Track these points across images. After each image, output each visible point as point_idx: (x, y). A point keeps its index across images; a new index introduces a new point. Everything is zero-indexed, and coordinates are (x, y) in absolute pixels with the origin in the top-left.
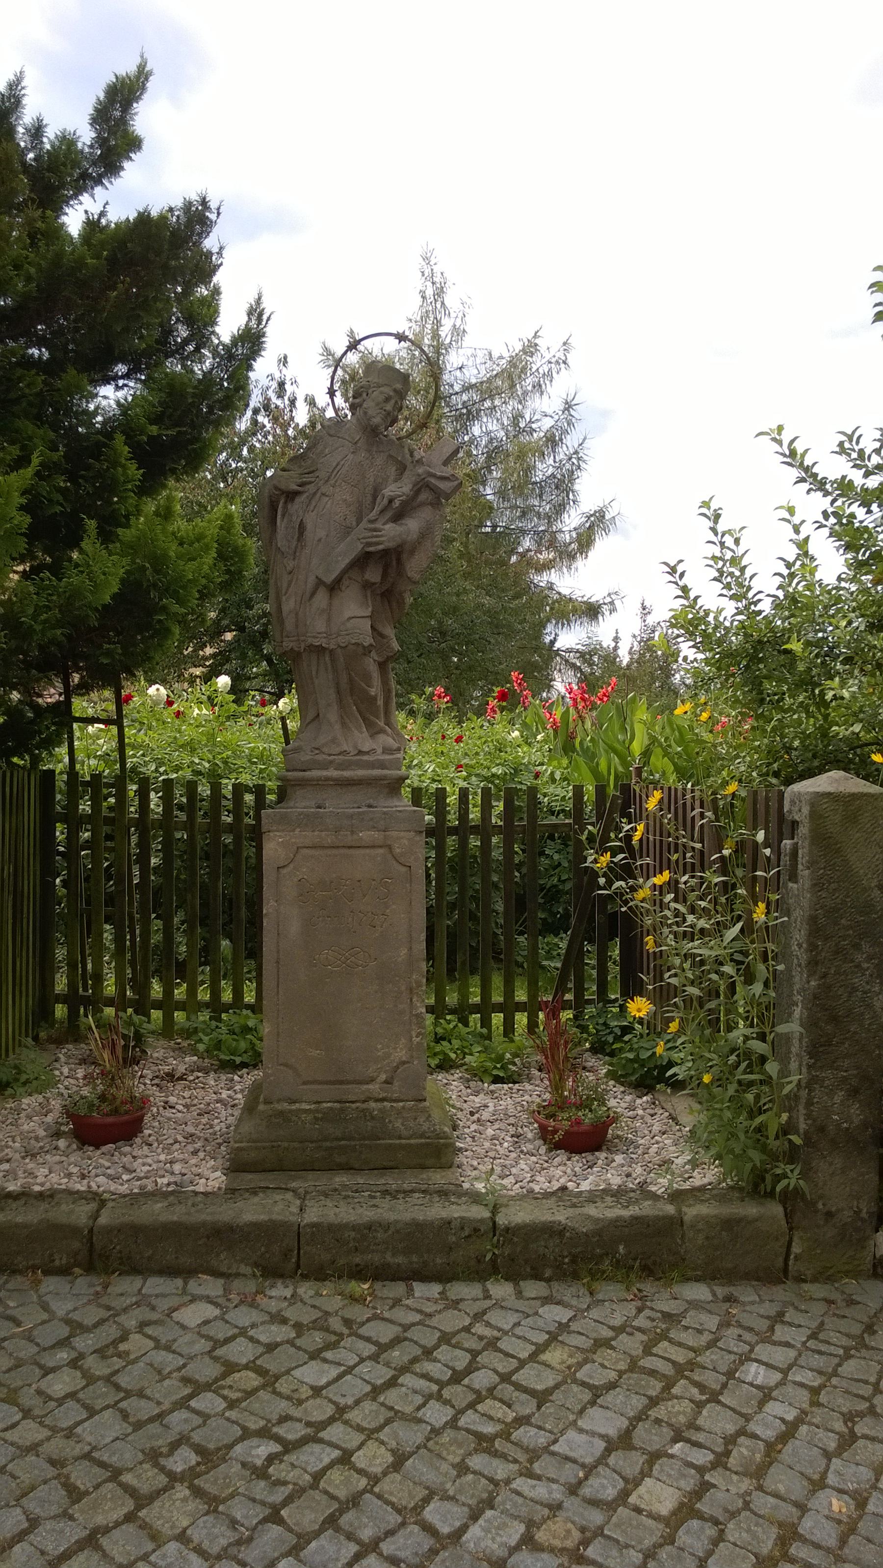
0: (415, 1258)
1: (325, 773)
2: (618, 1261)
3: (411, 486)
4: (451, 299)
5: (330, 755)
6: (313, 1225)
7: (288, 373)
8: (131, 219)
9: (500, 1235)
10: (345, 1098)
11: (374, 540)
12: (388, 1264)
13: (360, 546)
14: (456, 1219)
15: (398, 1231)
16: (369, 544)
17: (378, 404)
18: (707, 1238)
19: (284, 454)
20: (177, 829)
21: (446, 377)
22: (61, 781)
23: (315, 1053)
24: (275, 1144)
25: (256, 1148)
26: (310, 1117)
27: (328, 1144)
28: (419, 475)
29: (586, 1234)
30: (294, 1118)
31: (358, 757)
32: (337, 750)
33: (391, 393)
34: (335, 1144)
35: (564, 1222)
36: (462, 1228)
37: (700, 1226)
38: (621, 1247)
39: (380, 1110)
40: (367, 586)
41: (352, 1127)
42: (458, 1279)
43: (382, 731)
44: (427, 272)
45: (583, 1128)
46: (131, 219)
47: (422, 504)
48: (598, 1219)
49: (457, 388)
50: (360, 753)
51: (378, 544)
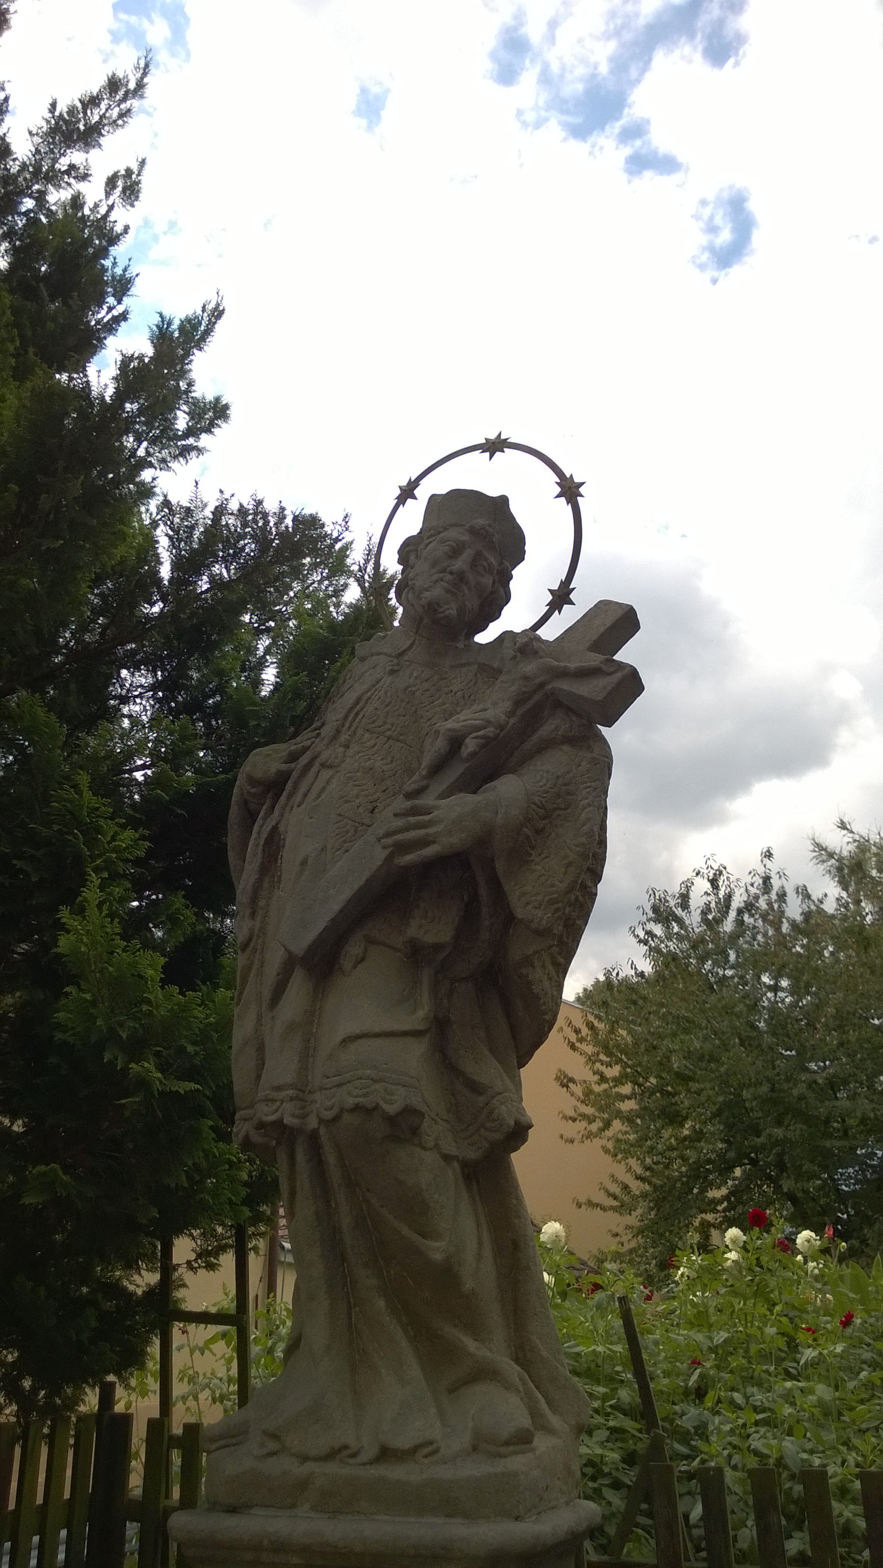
3: (507, 705)
5: (305, 1459)
7: (773, 866)
13: (380, 855)
16: (402, 848)
17: (434, 564)
22: (139, 1433)
28: (526, 678)
31: (374, 1471)
33: (466, 537)
40: (416, 954)
43: (484, 1373)
50: (385, 1454)
51: (425, 842)
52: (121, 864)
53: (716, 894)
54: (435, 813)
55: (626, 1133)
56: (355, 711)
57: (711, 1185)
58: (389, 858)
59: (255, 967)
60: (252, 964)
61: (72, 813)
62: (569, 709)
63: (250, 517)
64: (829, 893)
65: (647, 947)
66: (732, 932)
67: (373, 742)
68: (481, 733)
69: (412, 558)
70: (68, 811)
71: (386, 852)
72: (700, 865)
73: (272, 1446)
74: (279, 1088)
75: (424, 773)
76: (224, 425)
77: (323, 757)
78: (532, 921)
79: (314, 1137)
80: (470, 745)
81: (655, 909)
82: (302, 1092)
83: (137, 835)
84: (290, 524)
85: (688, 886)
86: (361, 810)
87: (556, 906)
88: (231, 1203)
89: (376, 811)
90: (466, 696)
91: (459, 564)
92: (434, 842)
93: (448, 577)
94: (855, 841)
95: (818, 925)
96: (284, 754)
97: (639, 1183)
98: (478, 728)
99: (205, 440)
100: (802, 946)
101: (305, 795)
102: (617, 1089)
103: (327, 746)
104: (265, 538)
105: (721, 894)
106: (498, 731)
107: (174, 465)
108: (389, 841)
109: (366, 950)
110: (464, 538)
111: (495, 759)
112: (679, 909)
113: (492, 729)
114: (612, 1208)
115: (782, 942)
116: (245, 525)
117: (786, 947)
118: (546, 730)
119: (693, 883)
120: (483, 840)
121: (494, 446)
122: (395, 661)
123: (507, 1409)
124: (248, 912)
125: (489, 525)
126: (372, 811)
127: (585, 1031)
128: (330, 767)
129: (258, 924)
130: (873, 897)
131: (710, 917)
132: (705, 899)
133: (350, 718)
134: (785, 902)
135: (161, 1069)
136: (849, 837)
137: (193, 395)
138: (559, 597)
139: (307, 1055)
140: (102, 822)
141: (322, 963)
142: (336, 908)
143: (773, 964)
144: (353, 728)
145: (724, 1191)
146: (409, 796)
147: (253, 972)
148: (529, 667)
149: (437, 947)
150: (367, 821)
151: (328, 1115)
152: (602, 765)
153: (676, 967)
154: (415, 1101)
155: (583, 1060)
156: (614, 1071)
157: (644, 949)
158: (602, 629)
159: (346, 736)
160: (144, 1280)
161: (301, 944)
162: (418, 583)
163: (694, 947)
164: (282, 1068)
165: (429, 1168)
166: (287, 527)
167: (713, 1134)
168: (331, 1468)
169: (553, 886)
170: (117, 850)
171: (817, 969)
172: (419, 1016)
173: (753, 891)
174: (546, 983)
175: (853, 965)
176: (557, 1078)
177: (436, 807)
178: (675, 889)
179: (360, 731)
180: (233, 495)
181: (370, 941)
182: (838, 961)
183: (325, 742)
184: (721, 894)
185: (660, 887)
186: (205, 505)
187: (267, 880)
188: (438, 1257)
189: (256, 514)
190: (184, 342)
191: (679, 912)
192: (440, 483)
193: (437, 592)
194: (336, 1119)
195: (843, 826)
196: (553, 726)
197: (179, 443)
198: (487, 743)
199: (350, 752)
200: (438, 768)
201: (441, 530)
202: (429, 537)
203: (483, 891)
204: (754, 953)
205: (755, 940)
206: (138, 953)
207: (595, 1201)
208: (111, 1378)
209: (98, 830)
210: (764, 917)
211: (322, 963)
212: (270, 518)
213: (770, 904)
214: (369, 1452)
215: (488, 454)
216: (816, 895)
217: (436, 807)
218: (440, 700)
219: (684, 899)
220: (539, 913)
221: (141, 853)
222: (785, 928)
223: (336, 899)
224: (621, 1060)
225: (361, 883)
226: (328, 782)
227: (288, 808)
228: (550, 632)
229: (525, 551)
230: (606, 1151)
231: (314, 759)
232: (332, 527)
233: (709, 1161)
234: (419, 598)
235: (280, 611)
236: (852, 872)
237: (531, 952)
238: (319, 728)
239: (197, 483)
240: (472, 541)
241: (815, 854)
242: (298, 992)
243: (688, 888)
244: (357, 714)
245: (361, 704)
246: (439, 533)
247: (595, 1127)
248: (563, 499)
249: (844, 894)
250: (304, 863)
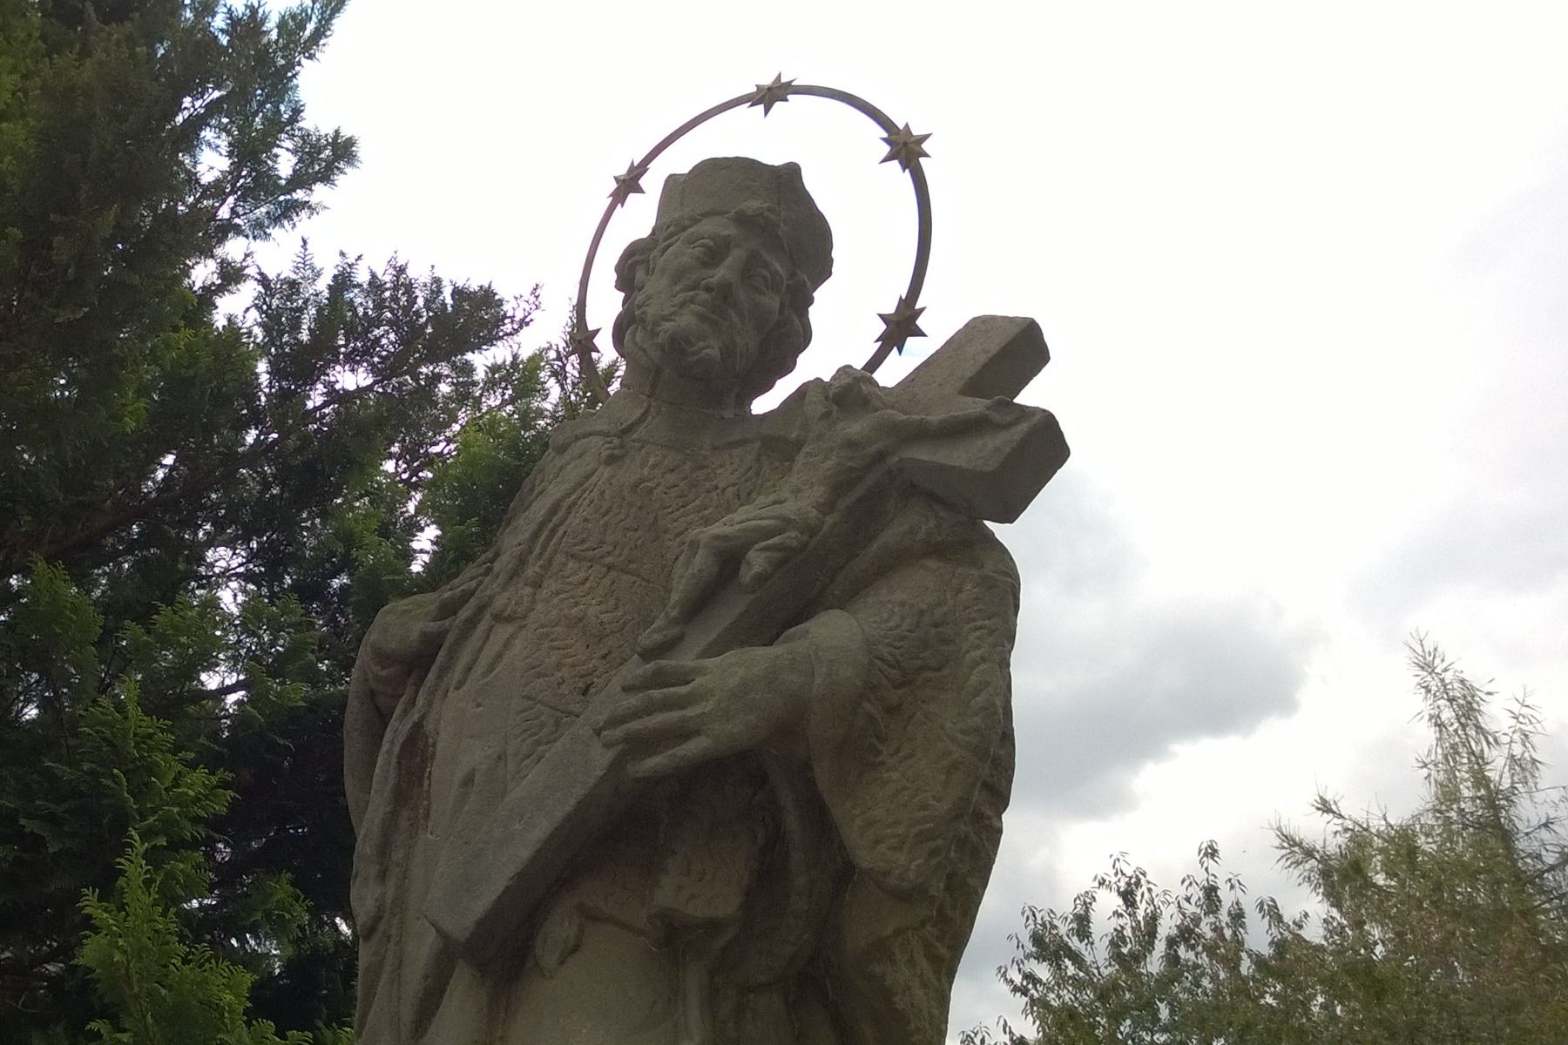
3: (819, 493)
4: (1496, 716)
7: (1221, 871)
13: (601, 758)
19: (1234, 1009)
21: (1521, 844)
28: (851, 444)
33: (731, 231)
40: (674, 939)
44: (1434, 685)
47: (888, 566)
49: (1550, 859)
51: (682, 733)
52: (188, 825)
53: (1133, 915)
54: (699, 681)
56: (551, 525)
58: (617, 765)
59: (388, 968)
60: (381, 964)
61: (110, 744)
62: (932, 498)
63: (387, 294)
64: (1311, 911)
65: (1025, 999)
66: (1162, 975)
67: (582, 575)
68: (776, 540)
69: (640, 274)
70: (104, 739)
71: (610, 755)
72: (1106, 870)
75: (674, 613)
76: (348, 170)
77: (499, 603)
78: (886, 874)
80: (757, 561)
81: (1037, 939)
83: (214, 779)
84: (449, 301)
85: (1087, 901)
86: (565, 689)
87: (932, 845)
89: (592, 690)
90: (743, 496)
91: (720, 274)
92: (697, 733)
93: (703, 296)
94: (1346, 830)
95: (1298, 959)
96: (432, 607)
98: (768, 533)
99: (320, 193)
100: (1275, 996)
101: (469, 669)
103: (504, 587)
104: (412, 324)
105: (1140, 914)
106: (805, 538)
107: (275, 232)
108: (618, 732)
109: (581, 931)
110: (726, 233)
111: (801, 585)
112: (1075, 939)
113: (793, 534)
115: (1241, 988)
116: (380, 306)
117: (1248, 996)
118: (891, 535)
120: (789, 726)
121: (770, 95)
122: (616, 441)
124: (373, 870)
125: (770, 210)
126: (585, 692)
128: (509, 619)
129: (391, 893)
130: (1381, 916)
131: (1125, 951)
133: (543, 537)
134: (1243, 925)
136: (1335, 824)
137: (301, 124)
138: (898, 324)
140: (157, 757)
141: (503, 952)
142: (525, 853)
143: (1230, 1024)
144: (546, 555)
146: (647, 655)
147: (385, 977)
148: (856, 427)
149: (713, 926)
150: (575, 708)
152: (1002, 588)
153: (1075, 1029)
158: (982, 359)
159: (537, 569)
161: (464, 918)
162: (652, 311)
163: (1103, 996)
166: (444, 304)
169: (924, 807)
170: (179, 801)
171: (1301, 1031)
173: (1191, 909)
174: (919, 993)
175: (1361, 1023)
177: (700, 671)
178: (1066, 906)
179: (560, 558)
180: (359, 257)
181: (591, 916)
182: (1334, 1018)
183: (500, 580)
184: (1140, 914)
185: (1042, 904)
186: (318, 275)
187: (405, 813)
189: (395, 288)
190: (286, 47)
191: (1074, 943)
192: (681, 159)
193: (686, 320)
195: (1325, 807)
196: (906, 527)
197: (282, 198)
198: (786, 558)
199: (544, 593)
200: (700, 604)
201: (687, 223)
202: (666, 239)
203: (792, 821)
204: (1199, 1007)
205: (1199, 986)
206: (207, 965)
209: (152, 769)
210: (1211, 950)
211: (503, 952)
212: (418, 292)
213: (1217, 929)
215: (761, 108)
216: (1289, 913)
217: (700, 671)
218: (697, 502)
219: (1082, 924)
220: (902, 858)
221: (221, 809)
222: (1246, 967)
225: (568, 809)
226: (507, 645)
227: (440, 693)
228: (891, 373)
229: (832, 260)
231: (481, 609)
232: (513, 303)
234: (654, 334)
235: (440, 454)
236: (1345, 878)
237: (889, 931)
239: (305, 242)
240: (737, 248)
241: (1284, 852)
243: (1087, 906)
244: (554, 531)
245: (560, 514)
246: (684, 229)
248: (895, 164)
249: (1335, 912)
250: (468, 781)
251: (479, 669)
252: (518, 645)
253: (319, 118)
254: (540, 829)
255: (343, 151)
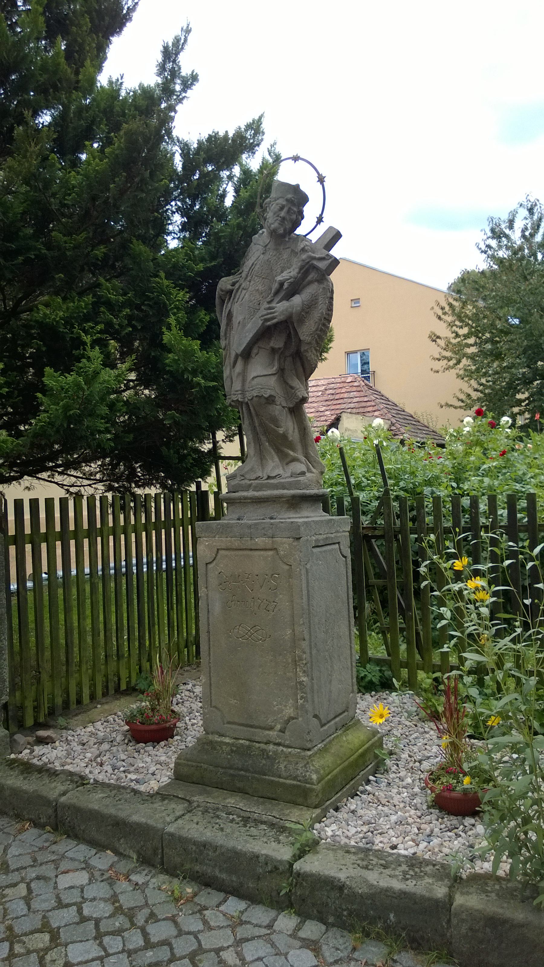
0: (234, 879)
1: (245, 494)
2: (389, 927)
3: (297, 270)
6: (171, 835)
8: (231, 135)
9: (294, 878)
10: (253, 738)
11: (269, 316)
12: (217, 877)
13: (261, 322)
14: (262, 855)
15: (223, 854)
18: (471, 929)
20: (520, 531)
23: (233, 702)
24: (199, 765)
25: (188, 765)
26: (228, 749)
27: (232, 772)
28: (303, 260)
29: (361, 896)
30: (218, 748)
31: (269, 481)
32: (254, 476)
33: (284, 203)
34: (236, 772)
35: (343, 880)
36: (267, 864)
37: (464, 916)
38: (392, 916)
39: (274, 752)
41: (250, 762)
42: (264, 904)
45: (453, 794)
46: (231, 135)
47: (310, 283)
48: (372, 885)
50: (269, 478)
53: (532, 218)
55: (469, 365)
57: (518, 392)
58: (263, 324)
65: (486, 256)
72: (523, 200)
73: (242, 478)
74: (237, 391)
79: (247, 404)
81: (493, 231)
82: (243, 392)
88: (234, 419)
91: (283, 214)
93: (280, 219)
97: (476, 392)
99: (189, 93)
102: (466, 341)
105: (535, 217)
111: (295, 288)
114: (461, 407)
118: (310, 278)
119: (517, 212)
123: (300, 467)
127: (447, 308)
132: (525, 222)
135: (203, 378)
139: (244, 381)
141: (246, 355)
142: (249, 339)
145: (527, 395)
149: (279, 349)
151: (250, 398)
154: (273, 393)
155: (445, 325)
156: (465, 330)
157: (484, 256)
160: (207, 447)
164: (237, 386)
165: (278, 410)
167: (519, 364)
168: (256, 481)
170: (178, 300)
172: (274, 370)
174: (313, 356)
176: (430, 337)
184: (535, 217)
185: (496, 216)
188: (281, 432)
191: (507, 231)
194: (252, 399)
199: (251, 284)
203: (292, 331)
207: (450, 403)
208: (200, 480)
209: (171, 294)
211: (246, 355)
214: (266, 477)
223: (248, 336)
224: (468, 324)
230: (458, 376)
231: (240, 286)
233: (518, 379)
238: (240, 273)
242: (239, 367)
243: (514, 216)
247: (451, 363)
250: (239, 323)
251: (240, 300)
252: (247, 296)
253: (185, 71)
254: (251, 335)
255: (194, 78)
